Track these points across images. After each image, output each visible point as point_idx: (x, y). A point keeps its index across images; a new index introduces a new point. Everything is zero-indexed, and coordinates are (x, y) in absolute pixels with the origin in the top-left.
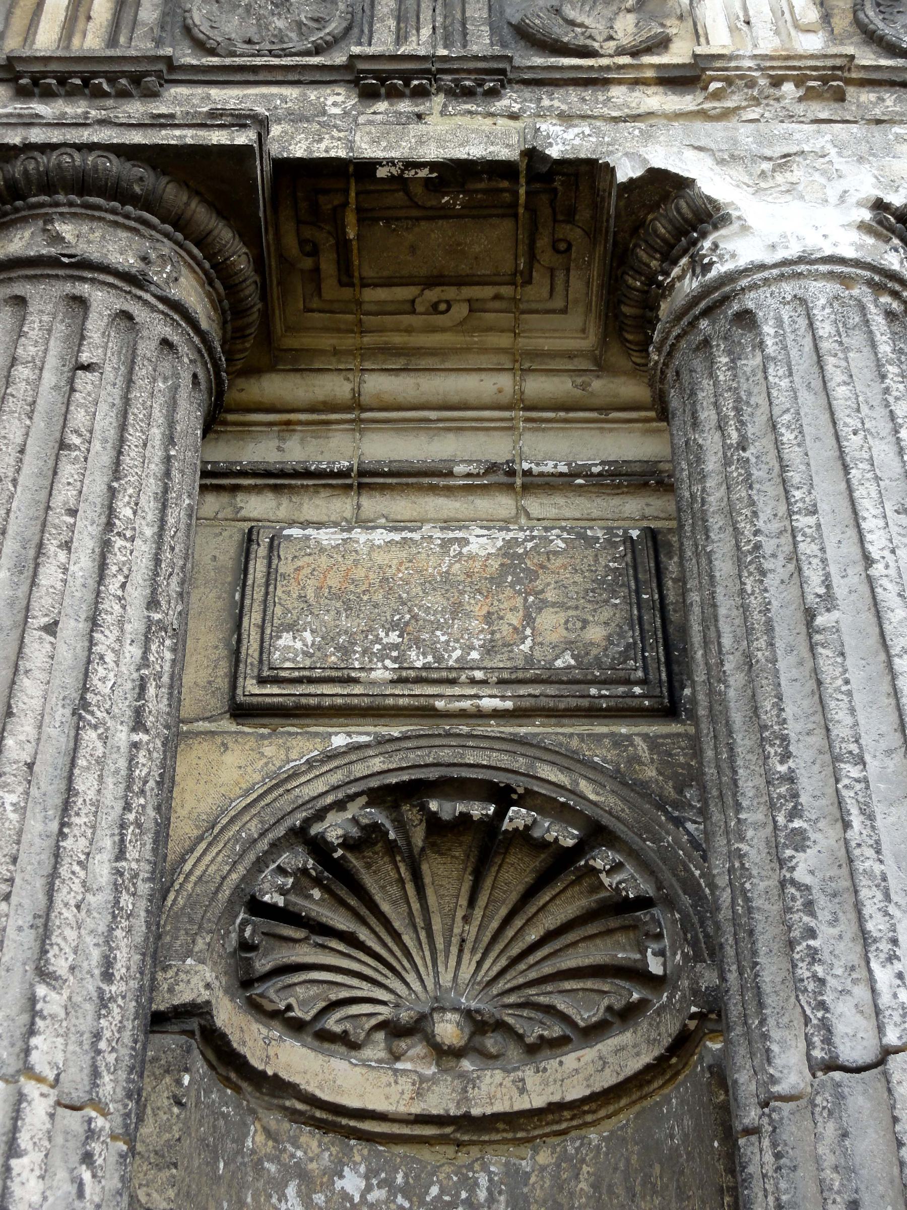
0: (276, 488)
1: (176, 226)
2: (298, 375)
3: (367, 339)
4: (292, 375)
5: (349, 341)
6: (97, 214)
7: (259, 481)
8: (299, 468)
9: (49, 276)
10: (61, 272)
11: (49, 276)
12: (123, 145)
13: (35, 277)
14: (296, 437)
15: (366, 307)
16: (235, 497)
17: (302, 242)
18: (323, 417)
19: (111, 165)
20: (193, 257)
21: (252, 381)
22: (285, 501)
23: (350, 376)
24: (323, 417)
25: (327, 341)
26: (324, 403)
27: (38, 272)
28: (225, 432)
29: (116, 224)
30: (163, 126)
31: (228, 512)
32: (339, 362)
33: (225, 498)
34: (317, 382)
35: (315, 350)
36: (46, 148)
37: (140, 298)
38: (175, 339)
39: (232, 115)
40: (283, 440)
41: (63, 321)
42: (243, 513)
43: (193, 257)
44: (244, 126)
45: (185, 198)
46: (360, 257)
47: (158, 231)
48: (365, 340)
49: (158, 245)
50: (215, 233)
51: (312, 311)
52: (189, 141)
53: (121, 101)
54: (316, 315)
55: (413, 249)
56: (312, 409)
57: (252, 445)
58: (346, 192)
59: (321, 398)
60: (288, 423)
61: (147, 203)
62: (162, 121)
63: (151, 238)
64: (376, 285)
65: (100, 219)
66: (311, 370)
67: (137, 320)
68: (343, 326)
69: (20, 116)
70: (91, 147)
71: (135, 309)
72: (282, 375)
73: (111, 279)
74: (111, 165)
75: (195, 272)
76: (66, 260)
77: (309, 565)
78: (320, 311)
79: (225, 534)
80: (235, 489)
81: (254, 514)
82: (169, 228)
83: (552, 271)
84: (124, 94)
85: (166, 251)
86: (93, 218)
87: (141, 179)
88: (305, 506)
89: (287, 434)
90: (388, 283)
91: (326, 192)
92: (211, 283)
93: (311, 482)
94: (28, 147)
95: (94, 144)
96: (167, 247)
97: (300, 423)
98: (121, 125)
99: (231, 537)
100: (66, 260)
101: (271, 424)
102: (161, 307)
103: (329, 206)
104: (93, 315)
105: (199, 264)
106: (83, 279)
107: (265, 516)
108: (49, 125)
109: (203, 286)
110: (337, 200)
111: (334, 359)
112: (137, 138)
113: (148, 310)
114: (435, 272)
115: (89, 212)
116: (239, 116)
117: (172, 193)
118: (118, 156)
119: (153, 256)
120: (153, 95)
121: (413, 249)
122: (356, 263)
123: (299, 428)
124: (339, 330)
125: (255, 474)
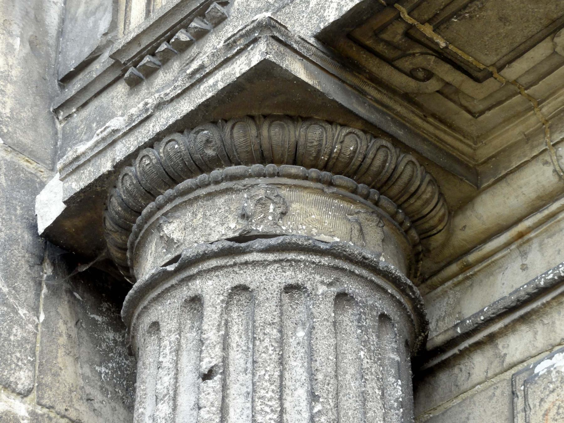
0: (523, 319)
1: (263, 160)
2: (503, 184)
3: (547, 109)
4: (498, 186)
5: (532, 121)
6: (191, 196)
7: (507, 320)
8: (531, 290)
9: (168, 290)
10: (174, 281)
11: (168, 290)
12: (177, 121)
13: (159, 296)
14: (535, 245)
15: (524, 81)
16: (496, 346)
17: (411, 74)
18: (546, 212)
19: (179, 144)
20: (295, 177)
21: (468, 213)
22: (539, 327)
23: (547, 158)
24: (546, 212)
25: (514, 132)
26: (539, 198)
27: (159, 291)
28: (475, 274)
29: (211, 196)
30: (200, 81)
31: (496, 367)
32: (532, 148)
33: (489, 351)
34: (522, 182)
35: (504, 150)
36: (129, 160)
37: (246, 263)
38: (300, 277)
39: (242, 36)
40: (524, 254)
41: (192, 327)
42: (509, 360)
43: (295, 177)
44: (255, 40)
45: (253, 131)
46: (468, 54)
47: (250, 176)
48: (544, 110)
49: (253, 192)
50: (302, 141)
51: (482, 113)
52: (221, 86)
53: (201, 42)
54: (488, 114)
55: (503, 19)
56: (534, 209)
57: (500, 276)
58: (398, 17)
59: (533, 196)
60: (521, 235)
61: (227, 158)
62: (198, 76)
63: (247, 188)
64: (510, 62)
65: (197, 198)
66: (512, 172)
67: (252, 287)
68: (520, 109)
69: (104, 139)
70: (158, 138)
71: (246, 277)
72: (491, 191)
73: (214, 263)
74: (179, 144)
75: (306, 188)
76: (171, 268)
77: (554, 404)
78: (489, 109)
79: (498, 392)
80: (492, 338)
81: (518, 356)
82: (257, 167)
83: (73, 387)
84: (201, 34)
85: (261, 193)
86: (190, 202)
87: (208, 141)
88: (557, 323)
89: (526, 247)
90: (518, 54)
91: (384, 28)
92: (330, 184)
93: (548, 298)
94: (118, 167)
95: (158, 134)
96: (262, 186)
97: (530, 229)
98: (172, 100)
99: (503, 393)
100: (171, 268)
101: (507, 245)
102: (270, 257)
103: (399, 37)
104: (208, 311)
105: (306, 178)
106: (191, 278)
107: (527, 354)
108: (125, 134)
109: (323, 192)
110: (400, 29)
111: (527, 148)
112: (186, 107)
113: (260, 269)
114: (545, 22)
115: (186, 198)
116: (248, 34)
117: (240, 136)
118: (182, 132)
119: (250, 206)
120: (221, 20)
121: (503, 19)
122: (471, 59)
123: (532, 235)
124: (518, 115)
125: (500, 316)
